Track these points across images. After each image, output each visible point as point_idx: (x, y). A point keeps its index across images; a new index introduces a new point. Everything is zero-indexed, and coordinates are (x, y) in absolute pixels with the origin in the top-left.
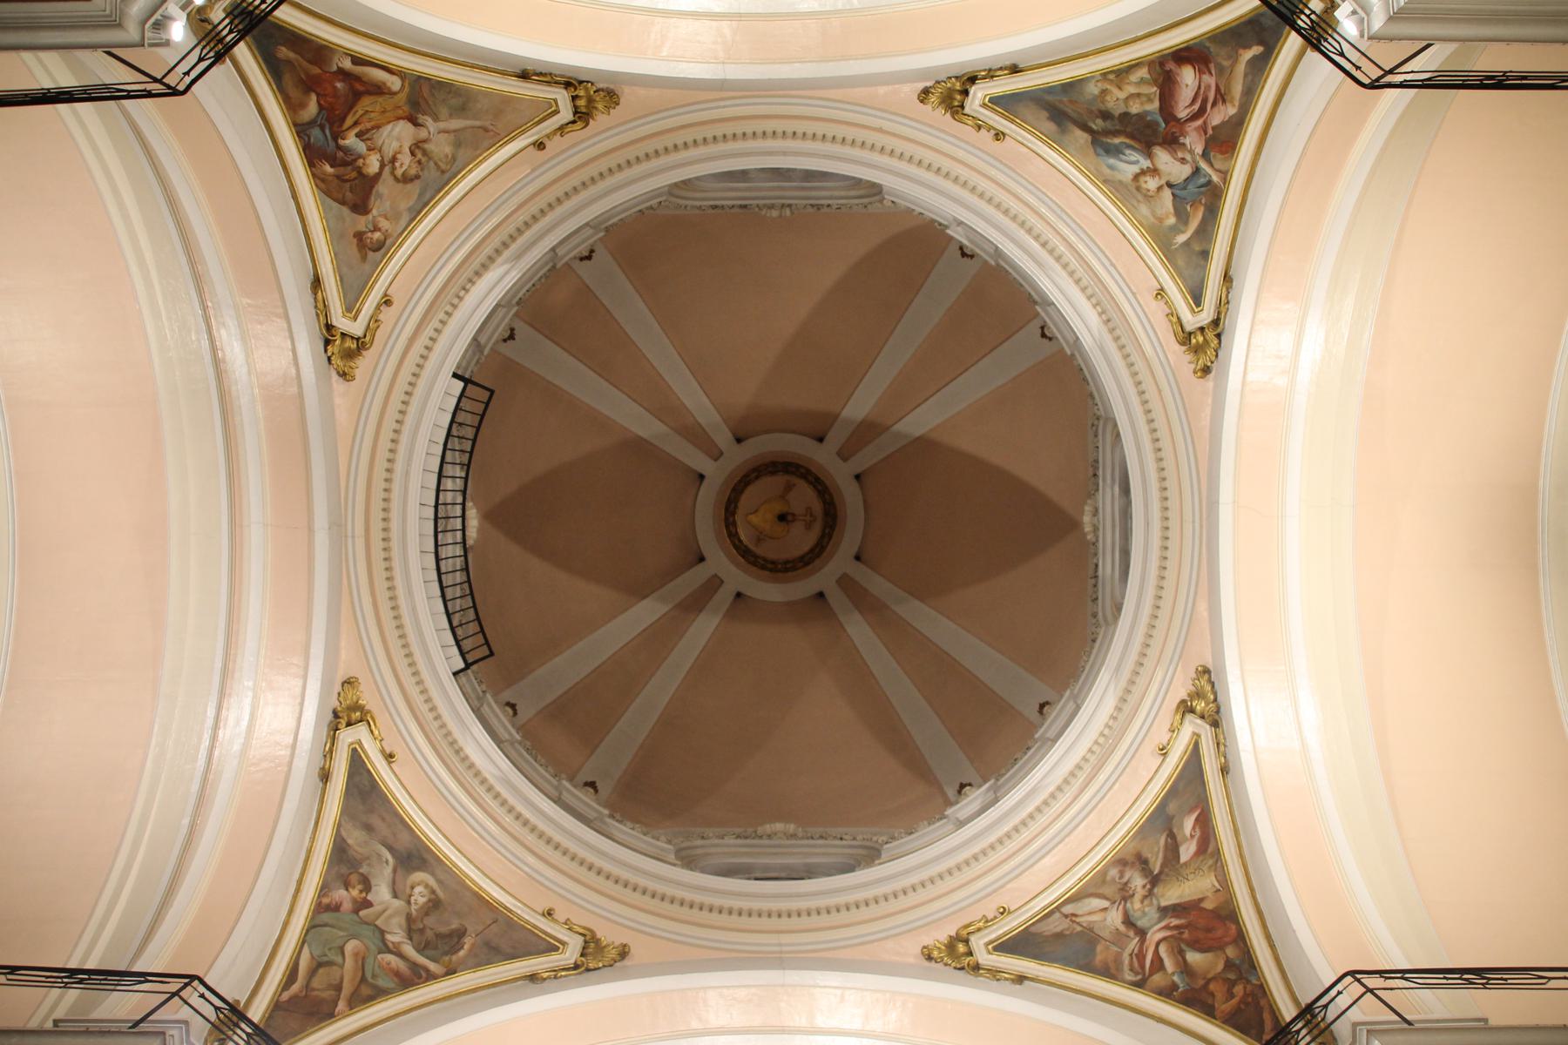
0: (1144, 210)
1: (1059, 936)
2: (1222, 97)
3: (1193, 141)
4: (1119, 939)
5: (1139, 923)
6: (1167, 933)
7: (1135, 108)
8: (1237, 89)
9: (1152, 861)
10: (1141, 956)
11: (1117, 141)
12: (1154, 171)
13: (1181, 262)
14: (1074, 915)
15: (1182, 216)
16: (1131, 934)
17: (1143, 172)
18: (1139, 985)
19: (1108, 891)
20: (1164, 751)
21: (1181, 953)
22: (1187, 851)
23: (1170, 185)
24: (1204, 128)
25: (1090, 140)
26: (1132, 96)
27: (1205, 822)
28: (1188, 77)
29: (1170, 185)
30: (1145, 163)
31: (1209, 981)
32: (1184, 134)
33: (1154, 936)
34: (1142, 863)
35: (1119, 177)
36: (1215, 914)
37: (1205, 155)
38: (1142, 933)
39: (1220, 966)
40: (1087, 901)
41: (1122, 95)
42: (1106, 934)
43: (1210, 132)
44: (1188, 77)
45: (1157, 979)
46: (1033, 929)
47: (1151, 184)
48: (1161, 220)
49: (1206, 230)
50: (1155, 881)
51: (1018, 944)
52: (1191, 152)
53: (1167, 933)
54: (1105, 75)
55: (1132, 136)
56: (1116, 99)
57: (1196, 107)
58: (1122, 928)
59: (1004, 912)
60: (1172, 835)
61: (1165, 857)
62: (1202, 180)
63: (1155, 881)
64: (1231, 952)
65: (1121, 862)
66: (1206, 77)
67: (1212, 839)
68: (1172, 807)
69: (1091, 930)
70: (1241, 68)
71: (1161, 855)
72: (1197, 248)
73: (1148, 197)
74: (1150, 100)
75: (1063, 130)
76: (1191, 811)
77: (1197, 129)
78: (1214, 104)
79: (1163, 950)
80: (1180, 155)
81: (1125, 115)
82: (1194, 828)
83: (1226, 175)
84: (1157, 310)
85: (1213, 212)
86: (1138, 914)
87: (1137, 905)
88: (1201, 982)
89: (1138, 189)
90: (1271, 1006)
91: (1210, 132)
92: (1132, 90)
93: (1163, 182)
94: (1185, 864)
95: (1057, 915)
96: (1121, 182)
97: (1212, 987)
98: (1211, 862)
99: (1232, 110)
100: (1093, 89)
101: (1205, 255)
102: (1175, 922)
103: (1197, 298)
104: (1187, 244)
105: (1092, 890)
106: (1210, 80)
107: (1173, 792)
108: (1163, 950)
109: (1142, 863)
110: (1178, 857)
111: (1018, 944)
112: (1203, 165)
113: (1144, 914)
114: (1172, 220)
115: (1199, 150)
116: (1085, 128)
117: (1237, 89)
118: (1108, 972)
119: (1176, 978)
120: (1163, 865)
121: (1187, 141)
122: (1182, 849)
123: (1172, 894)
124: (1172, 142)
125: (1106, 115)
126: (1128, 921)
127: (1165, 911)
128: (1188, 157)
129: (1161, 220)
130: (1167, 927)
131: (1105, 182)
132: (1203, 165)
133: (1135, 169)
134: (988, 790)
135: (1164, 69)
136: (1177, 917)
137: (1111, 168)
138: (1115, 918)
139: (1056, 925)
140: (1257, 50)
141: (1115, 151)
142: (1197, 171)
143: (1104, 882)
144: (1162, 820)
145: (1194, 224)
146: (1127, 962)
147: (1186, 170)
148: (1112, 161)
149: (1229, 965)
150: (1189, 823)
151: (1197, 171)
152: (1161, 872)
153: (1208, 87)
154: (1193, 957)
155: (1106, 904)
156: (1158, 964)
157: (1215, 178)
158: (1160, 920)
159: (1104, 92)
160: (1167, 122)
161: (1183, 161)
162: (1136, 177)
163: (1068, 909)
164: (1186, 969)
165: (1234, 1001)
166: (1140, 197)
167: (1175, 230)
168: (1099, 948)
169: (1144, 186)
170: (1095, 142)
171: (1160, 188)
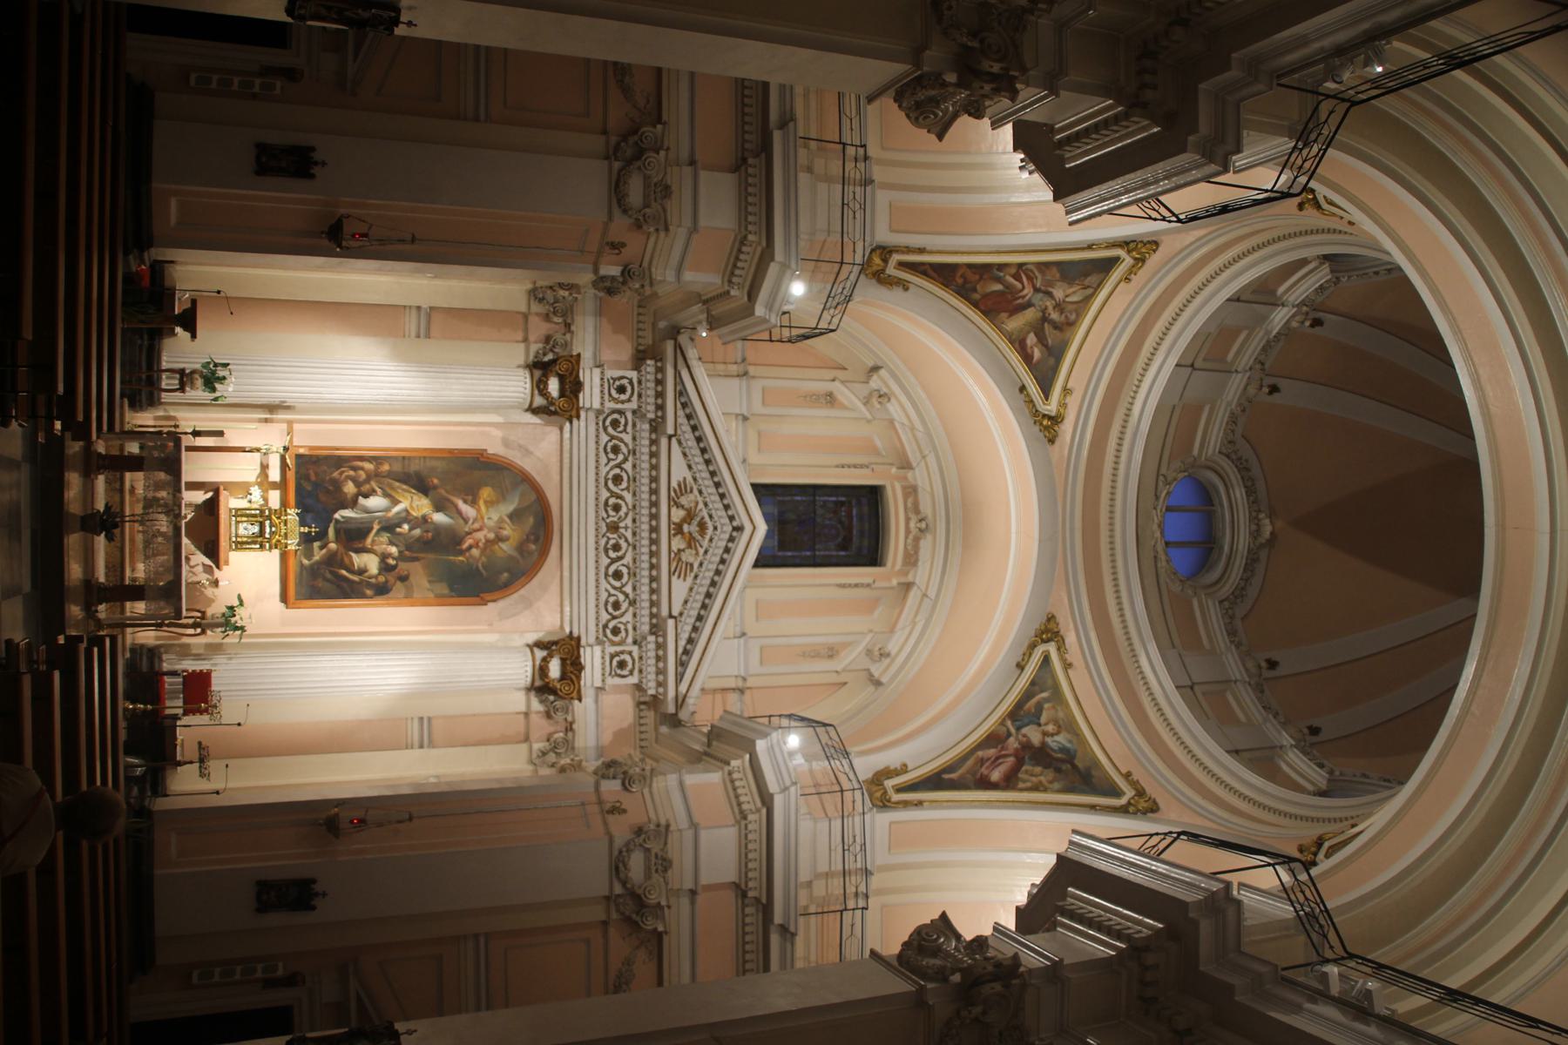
0: (1061, 714)
1: (1086, 275)
2: (982, 761)
3: (1013, 743)
4: (1051, 284)
5: (1041, 295)
6: (1021, 294)
7: (1038, 769)
8: (970, 762)
9: (1051, 329)
10: (1030, 279)
11: (1059, 755)
12: (1045, 734)
13: (1050, 682)
14: (1085, 288)
15: (1039, 708)
16: (1043, 288)
17: (1052, 735)
18: (1020, 265)
19: (1070, 307)
20: (1066, 391)
21: (1007, 287)
22: (1031, 339)
23: (1039, 725)
24: (1003, 749)
25: (625, 724)
26: (1036, 776)
27: (1027, 358)
28: (996, 776)
29: (1039, 725)
30: (1049, 740)
31: (981, 278)
32: (1017, 750)
33: (1028, 291)
34: (1056, 326)
35: (1069, 736)
36: (999, 311)
37: (1009, 735)
38: (1037, 290)
39: (978, 287)
40: (1081, 298)
41: (1042, 778)
42: (1059, 284)
43: (1000, 747)
44: (996, 776)
45: (1013, 271)
46: (1102, 275)
47: (1050, 728)
48: (1054, 707)
49: (1027, 695)
50: (1045, 318)
51: (1108, 265)
52: (1017, 739)
53: (1021, 294)
54: (1045, 790)
55: (1049, 756)
56: (1045, 776)
57: (1000, 761)
58: (1050, 289)
59: (1127, 279)
60: (1046, 346)
61: (1044, 333)
62: (1017, 723)
63: (1045, 318)
64: (976, 296)
65: (1071, 324)
66: (986, 772)
67: (1019, 349)
68: (1052, 361)
69: (1069, 283)
70: (960, 772)
71: (1047, 333)
72: (1037, 688)
73: (1056, 722)
74: (1026, 772)
75: (1088, 769)
76: (1039, 362)
77: (1007, 749)
78: (989, 759)
79: (1019, 286)
80: (1025, 739)
81: (1046, 767)
82: (1033, 352)
83: (1003, 723)
84: (1074, 655)
85: (1019, 705)
86: (1045, 299)
87: (1048, 303)
88: (985, 277)
89: (1059, 727)
90: (931, 278)
91: (1000, 747)
92: (1034, 779)
93: (1043, 728)
94: (1029, 332)
95: (1095, 286)
96: (1069, 732)
97: (977, 277)
98: (1014, 337)
99: (980, 753)
100: (1056, 786)
101: (1033, 683)
102: (1020, 301)
103: (1046, 660)
104: (1042, 691)
105: (1081, 305)
106: (984, 770)
107: (1055, 370)
108: (1019, 286)
109: (1056, 326)
110: (1036, 335)
111: (1108, 265)
112: (1013, 730)
113: (1041, 300)
114: (1046, 706)
115: (1012, 739)
116: (1074, 766)
117: (970, 762)
118: (1044, 266)
119: (1002, 274)
120: (1043, 328)
121: (1016, 745)
122: (1035, 340)
123: (1030, 315)
124: (1026, 746)
125: (1058, 770)
126: (1050, 294)
127: (1029, 305)
128: (1020, 737)
129: (1054, 707)
130: (1024, 297)
131: (1078, 735)
132: (1013, 730)
133: (1056, 738)
134: (1271, 332)
135: (1009, 782)
136: (1020, 304)
137: (1070, 742)
138: (1059, 293)
139: (1092, 280)
140: (946, 776)
141: (1063, 750)
142: (1018, 729)
143: (1076, 311)
144: (1056, 354)
145: (1034, 701)
146: (1037, 273)
147: (1025, 730)
148: (1068, 745)
149: (975, 290)
150: (1037, 354)
151: (1018, 729)
152: (1043, 324)
153: (987, 768)
154: (998, 287)
155: (1067, 299)
156: (1017, 277)
157: (1009, 723)
158: (1030, 299)
159: (1051, 782)
160: (1024, 758)
161: (1024, 736)
162: (1058, 733)
163: (1090, 291)
164: (999, 280)
165: (959, 274)
166: (1061, 722)
167: (1047, 700)
168: (1058, 275)
169: (1055, 728)
170: (1074, 757)
171: (1046, 724)
